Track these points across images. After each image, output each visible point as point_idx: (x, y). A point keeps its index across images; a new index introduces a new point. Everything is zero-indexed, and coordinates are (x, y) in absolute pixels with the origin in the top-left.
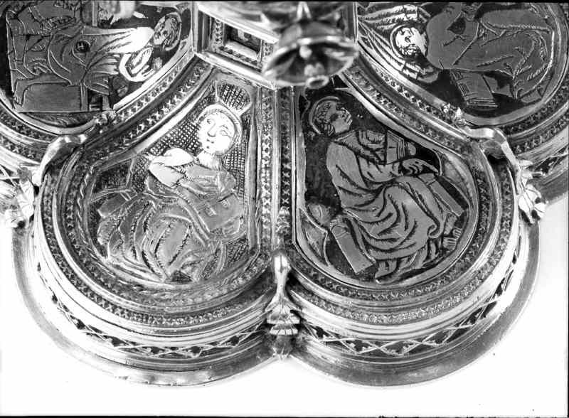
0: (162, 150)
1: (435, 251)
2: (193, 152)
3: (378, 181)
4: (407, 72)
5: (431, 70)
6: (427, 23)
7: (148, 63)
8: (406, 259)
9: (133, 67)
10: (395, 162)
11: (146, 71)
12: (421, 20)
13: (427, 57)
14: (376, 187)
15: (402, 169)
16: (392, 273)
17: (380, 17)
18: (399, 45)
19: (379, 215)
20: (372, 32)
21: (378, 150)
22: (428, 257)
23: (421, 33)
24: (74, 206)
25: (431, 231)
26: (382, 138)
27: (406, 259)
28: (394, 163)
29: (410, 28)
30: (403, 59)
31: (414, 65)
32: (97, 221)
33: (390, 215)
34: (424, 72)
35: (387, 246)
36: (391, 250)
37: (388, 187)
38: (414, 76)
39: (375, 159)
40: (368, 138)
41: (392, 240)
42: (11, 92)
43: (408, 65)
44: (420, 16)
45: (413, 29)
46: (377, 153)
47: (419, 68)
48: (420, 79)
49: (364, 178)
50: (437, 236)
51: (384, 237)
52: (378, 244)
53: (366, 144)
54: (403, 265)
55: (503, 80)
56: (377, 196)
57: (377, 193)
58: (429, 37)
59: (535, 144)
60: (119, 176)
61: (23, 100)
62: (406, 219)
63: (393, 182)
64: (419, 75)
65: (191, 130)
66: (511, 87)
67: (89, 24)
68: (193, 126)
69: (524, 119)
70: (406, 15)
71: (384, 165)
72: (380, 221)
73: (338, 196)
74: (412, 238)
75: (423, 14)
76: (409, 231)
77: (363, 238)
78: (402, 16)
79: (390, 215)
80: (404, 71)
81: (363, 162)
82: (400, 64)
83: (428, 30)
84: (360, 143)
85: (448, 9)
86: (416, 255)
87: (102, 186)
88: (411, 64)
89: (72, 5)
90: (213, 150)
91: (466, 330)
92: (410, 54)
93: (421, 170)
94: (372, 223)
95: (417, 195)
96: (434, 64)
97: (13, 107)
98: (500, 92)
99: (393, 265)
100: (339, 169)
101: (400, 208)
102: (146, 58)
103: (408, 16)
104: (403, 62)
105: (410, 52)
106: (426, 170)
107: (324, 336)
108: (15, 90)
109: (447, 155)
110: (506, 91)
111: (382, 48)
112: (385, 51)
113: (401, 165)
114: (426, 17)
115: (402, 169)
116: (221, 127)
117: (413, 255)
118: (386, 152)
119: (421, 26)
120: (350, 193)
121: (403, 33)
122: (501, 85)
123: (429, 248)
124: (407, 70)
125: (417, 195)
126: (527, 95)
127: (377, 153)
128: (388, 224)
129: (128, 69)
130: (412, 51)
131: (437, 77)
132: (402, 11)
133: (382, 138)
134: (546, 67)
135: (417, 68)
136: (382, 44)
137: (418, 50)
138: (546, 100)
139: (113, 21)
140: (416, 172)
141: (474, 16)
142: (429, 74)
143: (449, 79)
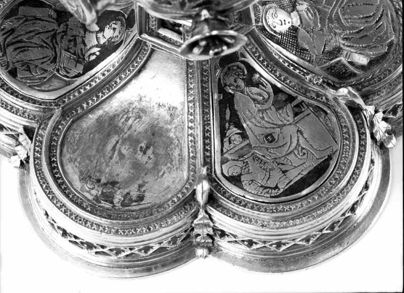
0: (305, 52)
2: (296, 31)
7: (258, 87)
9: (264, 98)
11: (264, 86)
24: (373, 79)
32: (374, 61)
42: (328, 158)
60: (336, 69)
61: (328, 148)
65: (285, 38)
67: (249, 145)
68: (281, 37)
87: (350, 73)
89: (244, 163)
90: (288, 20)
97: (336, 151)
102: (255, 90)
108: (325, 156)
109: (136, 24)
116: (274, 18)
129: (266, 101)
139: (239, 131)
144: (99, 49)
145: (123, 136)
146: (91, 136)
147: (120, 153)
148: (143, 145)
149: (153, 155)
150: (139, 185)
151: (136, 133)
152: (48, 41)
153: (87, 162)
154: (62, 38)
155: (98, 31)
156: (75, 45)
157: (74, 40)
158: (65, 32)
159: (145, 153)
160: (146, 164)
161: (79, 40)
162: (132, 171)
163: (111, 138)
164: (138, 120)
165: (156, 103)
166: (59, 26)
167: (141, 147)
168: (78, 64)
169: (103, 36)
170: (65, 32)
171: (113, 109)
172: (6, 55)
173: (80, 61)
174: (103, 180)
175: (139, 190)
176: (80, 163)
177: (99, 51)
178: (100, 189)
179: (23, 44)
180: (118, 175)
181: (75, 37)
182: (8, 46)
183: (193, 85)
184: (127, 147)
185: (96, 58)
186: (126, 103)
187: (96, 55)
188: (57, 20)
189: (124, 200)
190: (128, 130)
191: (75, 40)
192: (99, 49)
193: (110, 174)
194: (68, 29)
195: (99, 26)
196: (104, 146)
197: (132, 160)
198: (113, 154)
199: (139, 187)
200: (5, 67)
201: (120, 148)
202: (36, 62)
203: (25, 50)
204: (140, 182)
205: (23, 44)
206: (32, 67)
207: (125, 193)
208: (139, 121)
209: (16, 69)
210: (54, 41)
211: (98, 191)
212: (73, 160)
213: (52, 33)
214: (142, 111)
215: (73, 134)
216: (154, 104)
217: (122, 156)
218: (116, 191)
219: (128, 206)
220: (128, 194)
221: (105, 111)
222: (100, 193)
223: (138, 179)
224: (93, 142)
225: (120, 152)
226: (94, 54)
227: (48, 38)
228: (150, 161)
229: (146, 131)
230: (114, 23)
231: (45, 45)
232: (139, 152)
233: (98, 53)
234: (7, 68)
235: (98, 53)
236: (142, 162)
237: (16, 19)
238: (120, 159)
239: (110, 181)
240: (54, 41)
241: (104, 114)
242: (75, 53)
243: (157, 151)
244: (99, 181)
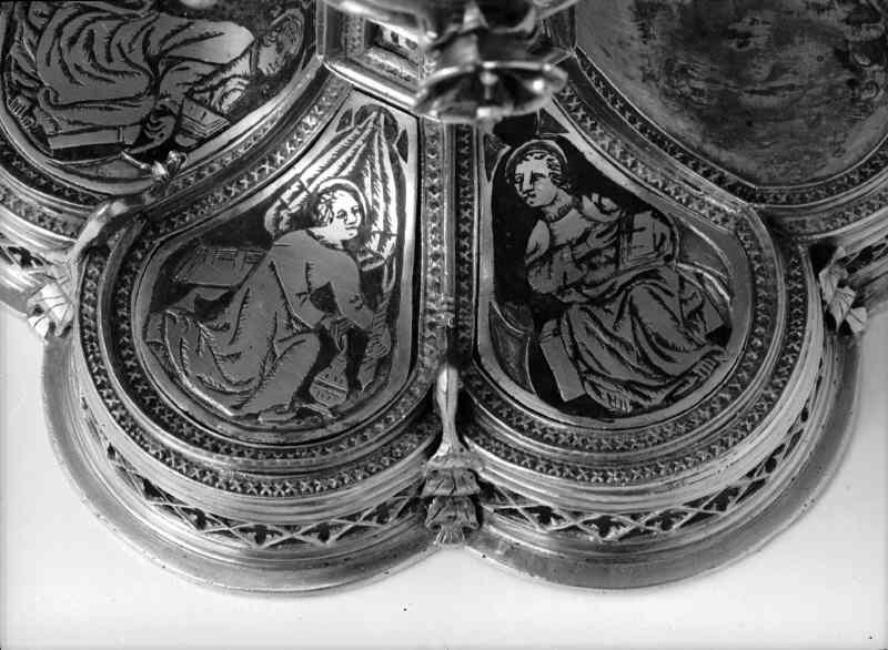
1: (22, 82)
3: (169, 74)
4: (294, 188)
5: (283, 226)
6: (355, 259)
8: (34, 42)
10: (180, 111)
12: (364, 253)
13: (304, 231)
14: (161, 68)
15: (165, 112)
16: (27, 13)
17: (384, 176)
18: (338, 193)
19: (119, 45)
20: (359, 142)
21: (212, 97)
22: (18, 68)
23: (345, 243)
25: (52, 94)
26: (225, 108)
27: (34, 42)
28: (181, 107)
29: (359, 228)
30: (316, 189)
31: (301, 205)
33: (110, 60)
34: (283, 213)
35: (69, 30)
36: (59, 33)
37: (151, 80)
38: (286, 196)
39: (201, 88)
40: (234, 90)
41: (73, 41)
43: (304, 195)
44: (370, 256)
45: (355, 232)
46: (208, 94)
47: (294, 211)
48: (278, 203)
49: (184, 59)
50: (40, 97)
51: (84, 34)
52: (78, 22)
53: (229, 83)
54: (29, 35)
55: (207, 311)
56: (147, 59)
57: (153, 62)
58: (333, 251)
59: (87, 297)
62: (90, 75)
63: (154, 89)
64: (284, 206)
66: (189, 314)
69: (132, 303)
70: (378, 232)
71: (186, 94)
72: (109, 43)
73: (182, 16)
74: (59, 66)
75: (371, 261)
76: (72, 70)
77: (97, 10)
78: (379, 225)
79: (110, 60)
80: (297, 184)
81: (208, 70)
82: (310, 181)
83: (344, 254)
84: (234, 76)
85: (361, 301)
86: (33, 57)
88: (305, 199)
91: (365, 529)
92: (320, 207)
93: (148, 134)
94: (113, 33)
95: (114, 106)
96: (288, 235)
98: (192, 296)
99: (39, 23)
100: (216, 35)
101: (112, 77)
103: (378, 236)
104: (311, 189)
105: (322, 208)
106: (142, 139)
107: (552, 519)
110: (188, 303)
111: (339, 154)
112: (332, 161)
113: (171, 113)
114: (364, 263)
115: (165, 112)
117: (35, 55)
118: (202, 105)
119: (354, 247)
120: (174, 33)
121: (354, 212)
122: (199, 302)
123: (29, 77)
124: (297, 189)
125: (114, 106)
126: (163, 326)
127: (208, 94)
128: (99, 50)
130: (323, 212)
131: (268, 229)
132: (389, 229)
133: (225, 108)
134: (187, 374)
135: (294, 207)
136: (343, 159)
137: (320, 224)
138: (141, 349)
140: (148, 125)
141: (327, 327)
142: (278, 220)
143: (255, 244)
144: (585, 198)
145: (735, 87)
146: (767, 143)
147: (773, 75)
148: (733, 45)
149: (744, 19)
150: (818, 13)
151: (715, 67)
152: (614, 307)
153: (824, 122)
154: (594, 285)
155: (546, 221)
156: (597, 252)
157: (588, 261)
158: (578, 286)
159: (748, 35)
160: (768, 23)
161: (582, 250)
162: (797, 39)
163: (751, 107)
164: (690, 71)
165: (645, 43)
166: (570, 305)
167: (740, 46)
168: (636, 227)
169: (552, 203)
170: (578, 286)
171: (692, 125)
172: (689, 369)
173: (627, 226)
174: (847, 75)
175: (829, 8)
176: (835, 133)
177: (590, 198)
178: (869, 71)
179: (648, 350)
180: (820, 59)
181: (578, 263)
182: (668, 376)
183: (287, 484)
184: (753, 71)
185: (606, 196)
186: (671, 104)
187: (600, 199)
188: (558, 317)
189: (867, 21)
190: (718, 83)
191: (583, 259)
192: (585, 198)
193: (825, 71)
194: (568, 283)
195: (535, 224)
196: (771, 111)
197: (775, 49)
198: (780, 88)
199: (823, 10)
200: (717, 358)
201: (761, 82)
202: (673, 303)
203: (659, 339)
204: (812, 14)
205: (648, 350)
206: (687, 310)
207: (849, 27)
208: (692, 70)
209: (709, 337)
210: (608, 296)
211: (874, 72)
212: (837, 148)
213: (593, 309)
214: (671, 69)
215: (782, 175)
216: (648, 47)
217: (776, 72)
218: (855, 43)
219: (873, 8)
220: (847, 21)
221: (704, 141)
222: (876, 67)
223: (809, 21)
224: (777, 135)
225: (770, 79)
226: (599, 205)
227: (607, 311)
228: (758, 18)
229: (703, 50)
230: (521, 186)
231: (627, 309)
232: (752, 45)
233: (595, 197)
234: (719, 353)
235: (595, 197)
236: (768, 33)
237: (599, 394)
238: (786, 71)
239: (840, 64)
240: (608, 296)
241: (709, 140)
242: (612, 245)
243: (732, 13)
244: (852, 83)
